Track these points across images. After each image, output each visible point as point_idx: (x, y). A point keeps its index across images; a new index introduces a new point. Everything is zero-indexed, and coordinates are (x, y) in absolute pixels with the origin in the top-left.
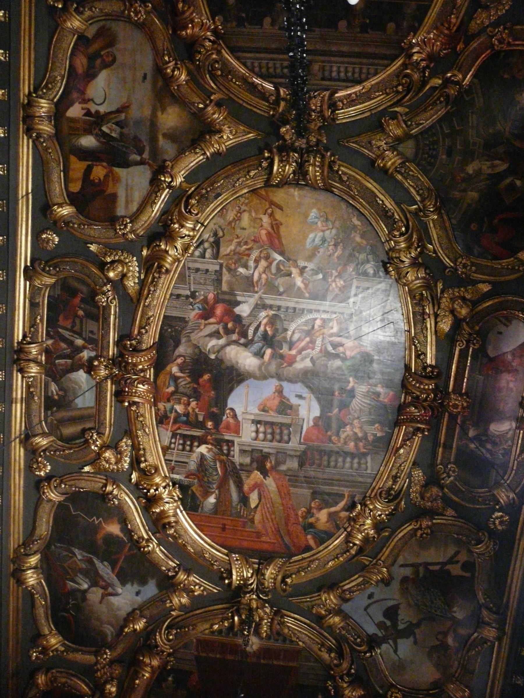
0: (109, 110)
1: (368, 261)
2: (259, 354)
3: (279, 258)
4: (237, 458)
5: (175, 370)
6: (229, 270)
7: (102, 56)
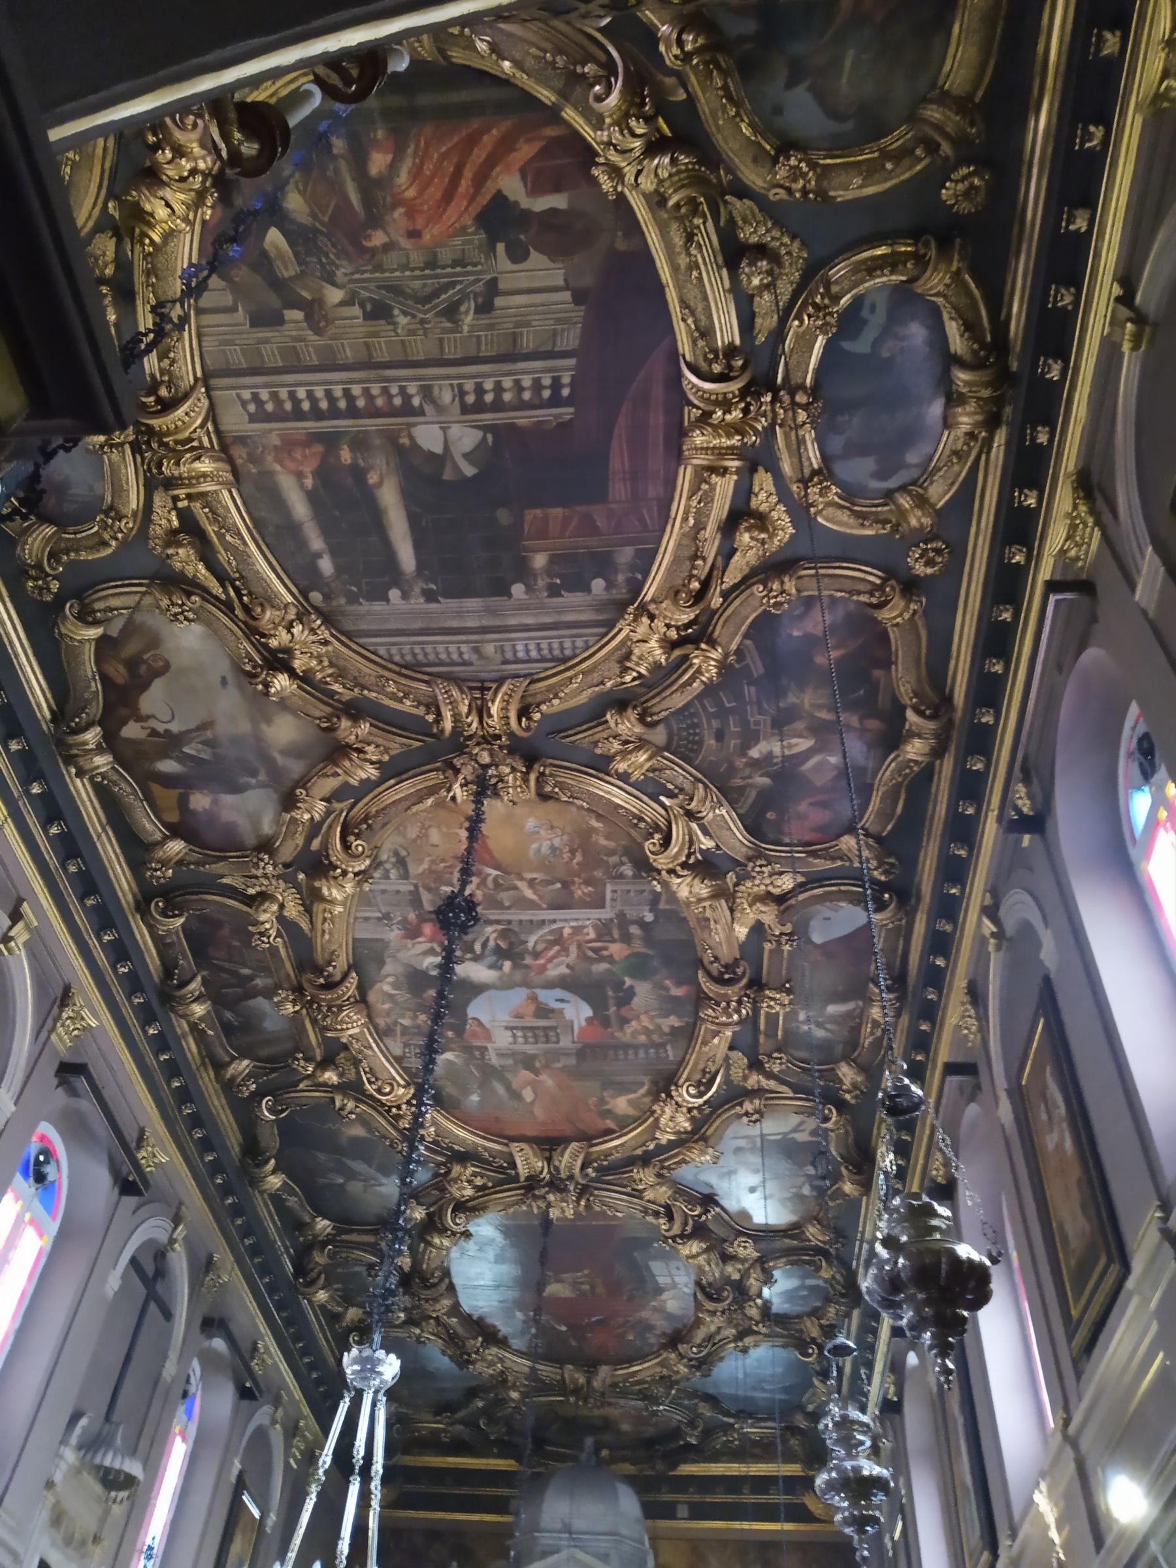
0: (184, 729)
1: (622, 864)
2: (493, 966)
3: (494, 873)
4: (494, 1060)
5: (387, 988)
6: (429, 890)
7: (145, 662)
